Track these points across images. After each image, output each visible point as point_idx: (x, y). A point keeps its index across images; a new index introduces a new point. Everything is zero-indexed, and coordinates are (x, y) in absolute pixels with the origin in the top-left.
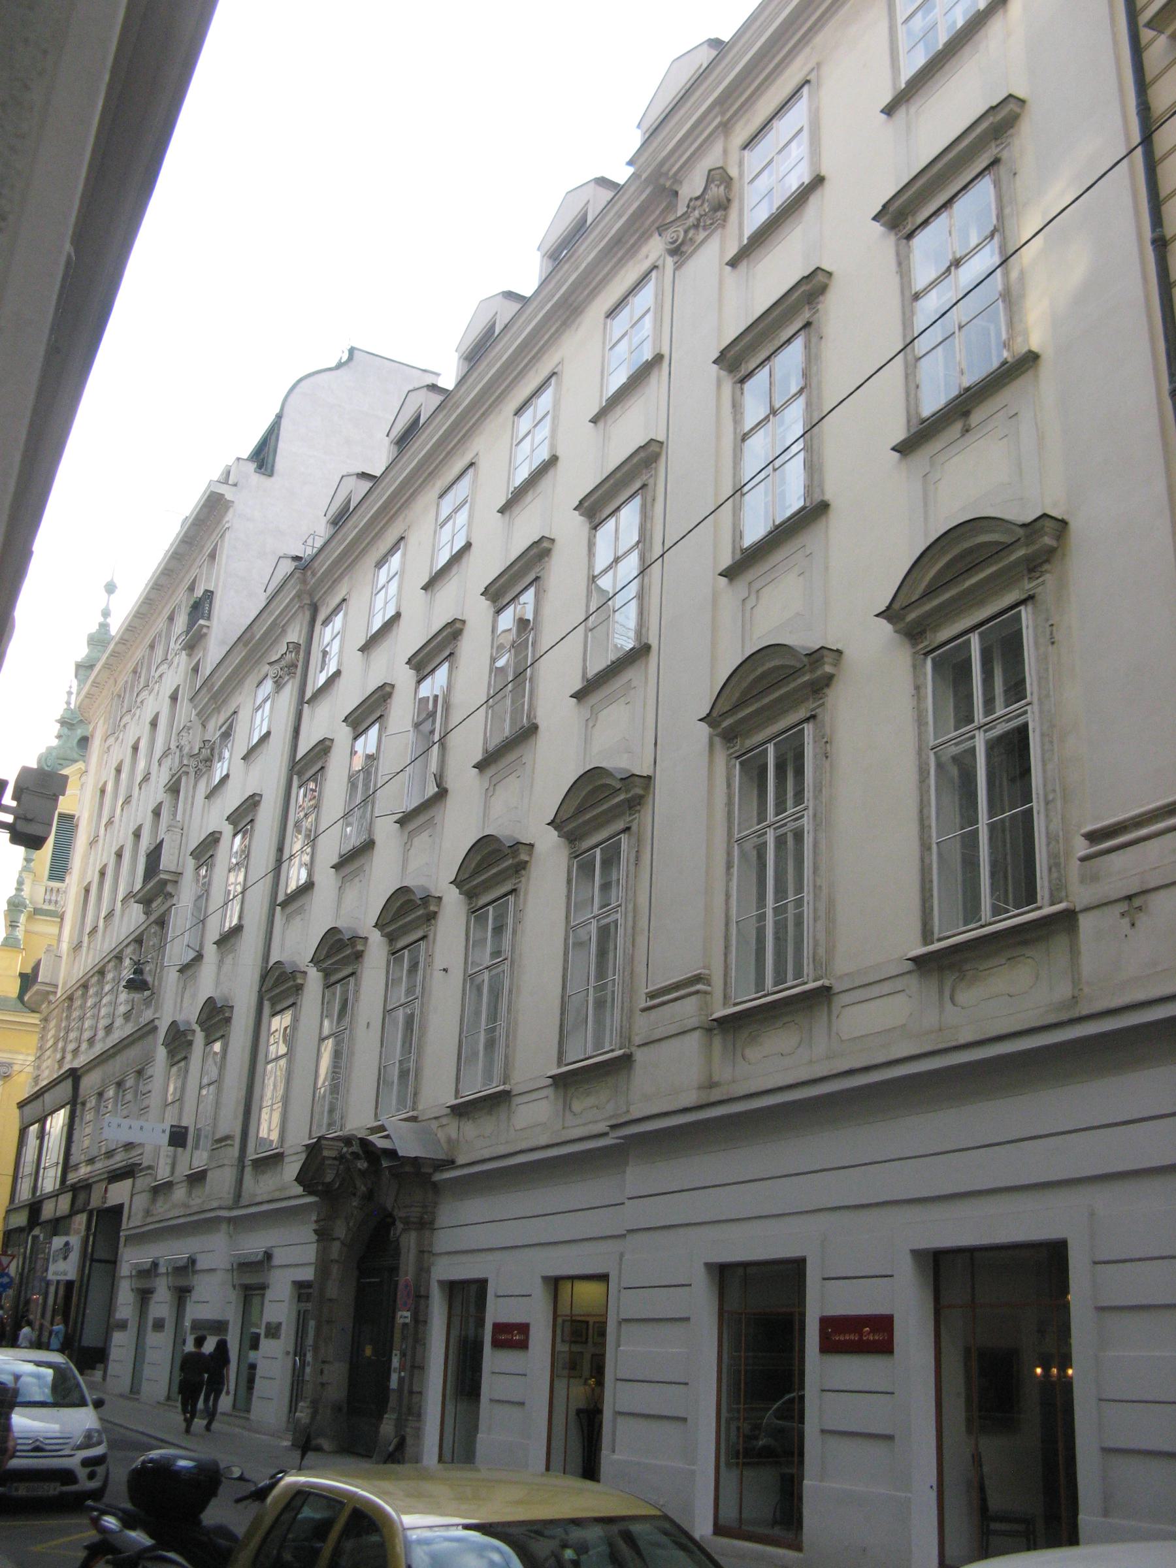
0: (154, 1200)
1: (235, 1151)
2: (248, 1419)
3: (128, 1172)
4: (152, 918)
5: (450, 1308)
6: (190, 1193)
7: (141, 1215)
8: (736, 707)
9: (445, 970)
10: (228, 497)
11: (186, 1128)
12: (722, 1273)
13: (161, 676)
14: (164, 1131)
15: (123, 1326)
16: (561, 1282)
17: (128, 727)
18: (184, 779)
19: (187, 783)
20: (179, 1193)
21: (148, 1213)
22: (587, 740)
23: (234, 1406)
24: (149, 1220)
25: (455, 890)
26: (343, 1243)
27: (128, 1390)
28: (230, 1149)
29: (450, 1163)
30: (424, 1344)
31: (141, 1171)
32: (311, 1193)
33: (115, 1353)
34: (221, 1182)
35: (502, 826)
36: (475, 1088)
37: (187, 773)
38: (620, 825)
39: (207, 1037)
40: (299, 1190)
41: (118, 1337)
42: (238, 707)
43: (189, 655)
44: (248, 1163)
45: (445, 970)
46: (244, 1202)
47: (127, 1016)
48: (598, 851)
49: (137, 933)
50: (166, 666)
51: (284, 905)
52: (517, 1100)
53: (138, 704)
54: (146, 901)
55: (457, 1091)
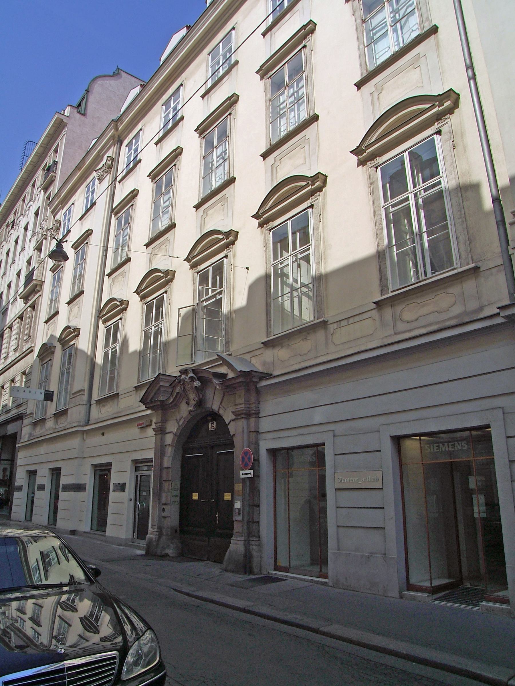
0: (34, 429)
1: (85, 398)
2: (105, 536)
3: (20, 417)
4: (28, 304)
5: (275, 467)
6: (56, 423)
7: (27, 436)
8: (43, 353)
9: (248, 268)
10: (65, 121)
11: (53, 392)
12: (95, 466)
13: (29, 208)
14: (41, 393)
15: (20, 489)
16: (401, 441)
17: (31, 207)
18: (44, 241)
19: (46, 243)
20: (50, 424)
21: (30, 435)
22: (151, 261)
23: (91, 529)
24: (31, 438)
25: (137, 298)
26: (175, 435)
27: (47, 523)
28: (83, 396)
29: (269, 376)
30: (259, 491)
31: (26, 416)
32: (148, 408)
33: (15, 502)
34: (76, 414)
35: (162, 263)
36: (107, 393)
37: (46, 239)
38: (222, 255)
39: (63, 347)
40: (143, 407)
41: (16, 494)
42: (75, 201)
43: (45, 193)
44: (93, 402)
45: (248, 268)
46: (90, 423)
47: (15, 350)
48: (155, 300)
49: (20, 314)
50: (32, 203)
51: (109, 275)
52: (47, 421)
53: (9, 235)
54: (26, 298)
55: (138, 380)
